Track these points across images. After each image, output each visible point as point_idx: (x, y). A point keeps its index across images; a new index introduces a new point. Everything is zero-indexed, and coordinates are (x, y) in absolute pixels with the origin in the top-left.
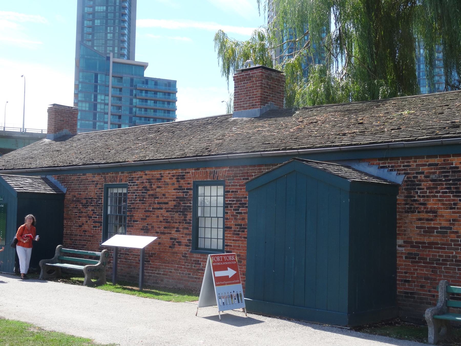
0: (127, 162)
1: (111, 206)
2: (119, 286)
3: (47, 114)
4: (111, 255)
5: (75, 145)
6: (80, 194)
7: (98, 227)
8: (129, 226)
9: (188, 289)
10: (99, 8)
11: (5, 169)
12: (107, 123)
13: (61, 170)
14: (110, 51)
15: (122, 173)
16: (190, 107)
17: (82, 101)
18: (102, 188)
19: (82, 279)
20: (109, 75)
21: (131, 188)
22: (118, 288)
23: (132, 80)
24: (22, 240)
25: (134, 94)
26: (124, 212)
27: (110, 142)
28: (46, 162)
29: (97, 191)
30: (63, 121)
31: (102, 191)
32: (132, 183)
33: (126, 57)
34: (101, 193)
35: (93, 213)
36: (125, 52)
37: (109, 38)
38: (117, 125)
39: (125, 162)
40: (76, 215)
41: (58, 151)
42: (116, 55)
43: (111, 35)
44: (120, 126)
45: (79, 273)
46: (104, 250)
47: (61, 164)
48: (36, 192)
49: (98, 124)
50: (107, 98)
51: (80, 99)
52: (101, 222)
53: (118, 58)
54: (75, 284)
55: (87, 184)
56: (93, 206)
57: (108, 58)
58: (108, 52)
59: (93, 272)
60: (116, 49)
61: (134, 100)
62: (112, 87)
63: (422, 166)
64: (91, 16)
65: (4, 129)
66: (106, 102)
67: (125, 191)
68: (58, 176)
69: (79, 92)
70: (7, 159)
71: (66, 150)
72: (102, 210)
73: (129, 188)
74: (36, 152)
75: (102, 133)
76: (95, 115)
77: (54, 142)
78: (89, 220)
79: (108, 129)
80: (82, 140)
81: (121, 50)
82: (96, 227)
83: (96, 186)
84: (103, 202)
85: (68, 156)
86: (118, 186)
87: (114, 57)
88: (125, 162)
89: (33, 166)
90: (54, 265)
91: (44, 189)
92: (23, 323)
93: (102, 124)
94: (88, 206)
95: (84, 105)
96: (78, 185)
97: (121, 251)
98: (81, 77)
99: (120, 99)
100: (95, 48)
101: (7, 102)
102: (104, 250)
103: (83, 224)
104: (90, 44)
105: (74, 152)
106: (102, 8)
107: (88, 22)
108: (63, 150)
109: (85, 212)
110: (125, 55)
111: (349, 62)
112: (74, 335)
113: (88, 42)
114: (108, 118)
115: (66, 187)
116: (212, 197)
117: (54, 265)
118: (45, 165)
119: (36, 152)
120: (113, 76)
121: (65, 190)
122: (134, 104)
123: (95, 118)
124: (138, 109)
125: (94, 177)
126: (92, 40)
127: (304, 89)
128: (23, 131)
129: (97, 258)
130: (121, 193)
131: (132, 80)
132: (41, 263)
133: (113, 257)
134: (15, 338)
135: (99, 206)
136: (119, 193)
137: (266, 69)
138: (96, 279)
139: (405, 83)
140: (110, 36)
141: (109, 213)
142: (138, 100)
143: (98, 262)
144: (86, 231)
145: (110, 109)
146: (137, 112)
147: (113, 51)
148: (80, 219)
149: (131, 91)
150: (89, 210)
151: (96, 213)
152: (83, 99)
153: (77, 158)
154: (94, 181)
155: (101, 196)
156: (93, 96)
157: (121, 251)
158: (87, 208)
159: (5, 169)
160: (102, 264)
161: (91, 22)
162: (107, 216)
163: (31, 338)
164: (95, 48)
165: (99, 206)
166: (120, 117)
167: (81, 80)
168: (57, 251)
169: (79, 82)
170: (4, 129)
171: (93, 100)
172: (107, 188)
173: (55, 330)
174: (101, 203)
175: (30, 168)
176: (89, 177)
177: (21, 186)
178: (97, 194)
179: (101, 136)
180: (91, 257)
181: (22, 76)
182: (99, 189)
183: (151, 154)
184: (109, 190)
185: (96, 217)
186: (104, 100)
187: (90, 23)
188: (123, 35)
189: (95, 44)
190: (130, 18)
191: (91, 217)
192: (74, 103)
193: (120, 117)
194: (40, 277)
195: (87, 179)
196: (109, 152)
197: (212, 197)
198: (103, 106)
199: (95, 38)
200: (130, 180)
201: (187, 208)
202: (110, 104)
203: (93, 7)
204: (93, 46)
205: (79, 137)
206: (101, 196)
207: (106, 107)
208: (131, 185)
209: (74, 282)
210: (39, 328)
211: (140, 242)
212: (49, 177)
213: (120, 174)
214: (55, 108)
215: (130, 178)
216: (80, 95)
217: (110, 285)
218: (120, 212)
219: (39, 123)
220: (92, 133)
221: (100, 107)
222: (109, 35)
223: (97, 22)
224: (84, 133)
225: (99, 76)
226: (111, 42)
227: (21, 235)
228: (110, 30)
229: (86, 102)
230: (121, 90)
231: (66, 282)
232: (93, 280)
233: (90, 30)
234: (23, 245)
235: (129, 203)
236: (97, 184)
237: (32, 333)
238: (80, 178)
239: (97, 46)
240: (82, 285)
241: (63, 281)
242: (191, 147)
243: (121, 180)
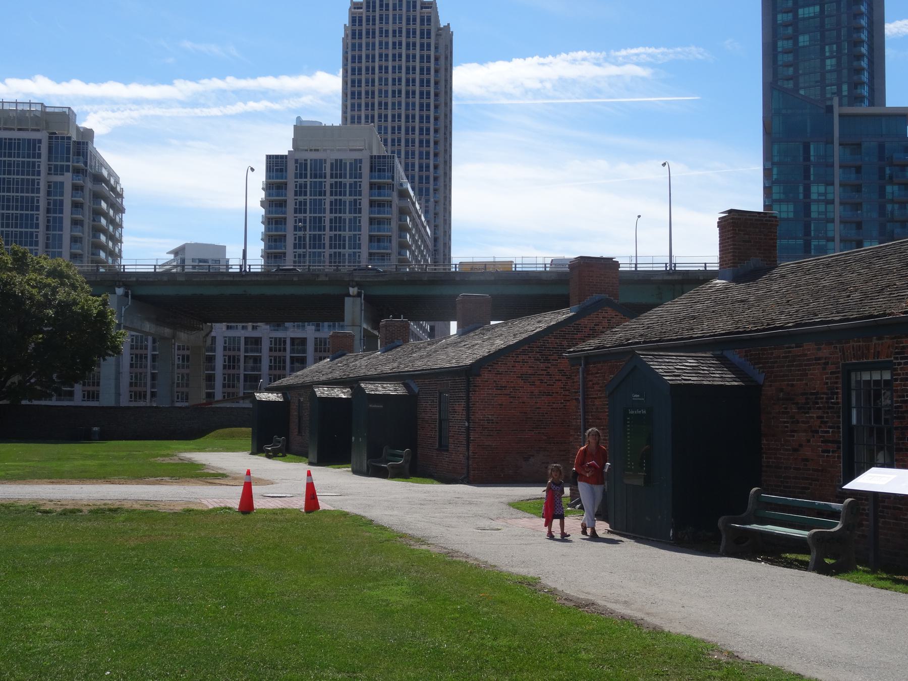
0: (890, 315)
1: (859, 408)
2: (885, 576)
3: (717, 231)
4: (864, 509)
5: (775, 287)
6: (792, 385)
7: (833, 452)
8: (899, 450)
10: (806, 9)
11: (645, 342)
12: (832, 239)
13: (752, 339)
14: (834, 93)
15: (879, 339)
17: (779, 201)
18: (838, 372)
19: (806, 558)
20: (832, 143)
21: (901, 369)
22: (883, 579)
23: (881, 147)
24: (583, 473)
25: (887, 176)
26: (886, 421)
27: (849, 276)
28: (722, 325)
29: (827, 378)
31: (837, 378)
32: (902, 358)
33: (866, 102)
34: (836, 383)
35: (822, 422)
36: (865, 91)
37: (828, 68)
38: (854, 243)
39: (885, 315)
40: (787, 427)
41: (742, 301)
42: (845, 100)
43: (834, 61)
44: (860, 244)
45: (798, 545)
46: (850, 500)
47: (750, 327)
48: (705, 383)
49: (814, 243)
50: (830, 188)
51: (775, 196)
52: (839, 442)
53: (850, 104)
54: (791, 568)
55: (806, 365)
56: (819, 408)
57: (830, 109)
58: (828, 96)
59: (824, 543)
60: (845, 87)
61: (889, 189)
62: (841, 167)
64: (790, 30)
65: (636, 267)
66: (830, 197)
67: (887, 376)
68: (746, 352)
69: (773, 183)
70: (646, 322)
71: (759, 299)
72: (839, 417)
73: (896, 370)
74: (699, 306)
75: (830, 260)
76: (807, 227)
77: (732, 285)
78: (813, 436)
79: (835, 253)
80: (790, 276)
81: (856, 88)
82: (828, 452)
83: (824, 369)
84: (840, 401)
85: (764, 311)
86: (871, 367)
87: (841, 105)
88: (885, 315)
89: (698, 333)
90: (748, 527)
91: (720, 377)
92: (697, 641)
93: (823, 242)
94: (809, 408)
95: (784, 207)
96: (788, 366)
97: (884, 502)
98: (775, 152)
99: (858, 188)
100: (802, 92)
101: (639, 216)
102: (850, 500)
103: (801, 446)
104: (790, 85)
105: (772, 303)
106: (811, 9)
107: (785, 42)
108: (752, 298)
109: (803, 422)
110: (864, 97)
111: (204, 404)
112: (802, 674)
113: (786, 82)
114: (836, 230)
115: (763, 372)
117: (748, 527)
118: (719, 331)
119: (699, 306)
120: (840, 145)
121: (761, 378)
122: (889, 196)
123: (807, 232)
124: (896, 206)
125: (819, 349)
126: (794, 78)
128: (671, 269)
129: (835, 514)
130: (869, 381)
131: (881, 147)
132: (720, 522)
133: (867, 515)
134: (686, 670)
135: (833, 408)
136: (885, 381)
138: (834, 556)
140: (830, 63)
141: (854, 422)
142: (896, 188)
143: (836, 524)
144: (807, 460)
145: (837, 211)
146: (896, 213)
147: (839, 93)
148: (793, 436)
149: (882, 170)
150: (812, 417)
151: (826, 422)
152: (782, 196)
153: (782, 313)
154: (819, 359)
155: (837, 388)
156: (801, 189)
157: (884, 502)
158: (808, 413)
159: (645, 342)
160: (845, 527)
161: (791, 42)
162: (850, 429)
163: (715, 673)
164: (802, 92)
165: (833, 408)
166: (859, 225)
167: (776, 159)
168: (751, 500)
169: (773, 164)
170: (636, 267)
171: (801, 196)
172: (848, 370)
173: (763, 660)
174: (838, 403)
175: (691, 338)
176: (809, 350)
177: (677, 372)
178: (827, 383)
179: (828, 265)
180: (821, 512)
181: (664, 164)
182: (832, 373)
184: (853, 375)
185: (827, 432)
186: (825, 194)
187: (789, 44)
188: (860, 57)
189: (801, 85)
190: (871, 23)
191: (817, 432)
192: (765, 206)
193: (859, 225)
194: (721, 550)
195: (806, 355)
196: (849, 296)
198: (822, 208)
199: (801, 72)
200: (897, 353)
202: (837, 201)
203: (794, 11)
204: (797, 88)
205: (783, 271)
206: (837, 388)
207: (830, 207)
208: (900, 364)
209: (788, 563)
210: (729, 653)
212: (726, 353)
213: (875, 341)
214: (732, 219)
215: (896, 348)
216: (775, 189)
217: (864, 571)
218: (878, 419)
219: (701, 249)
220: (809, 262)
221: (815, 210)
222: (828, 62)
223: (804, 40)
224: (791, 264)
225: (812, 147)
226: (834, 75)
227: (581, 464)
228: (831, 51)
229: (786, 201)
230: (858, 170)
231: (773, 563)
232: (827, 561)
233: (790, 58)
234: (587, 480)
235: (897, 402)
236: (826, 364)
237: (718, 662)
238: (790, 352)
239: (804, 88)
240: (806, 570)
241: (766, 561)
243: (878, 354)
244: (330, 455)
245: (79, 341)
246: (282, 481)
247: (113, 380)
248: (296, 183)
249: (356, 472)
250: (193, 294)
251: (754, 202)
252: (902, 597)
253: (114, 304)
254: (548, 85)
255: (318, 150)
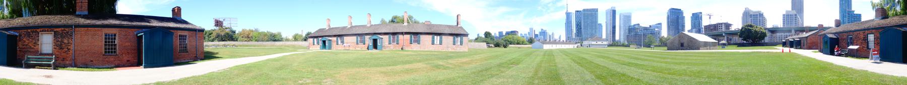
9: (867, 57)
16: (864, 18)
30: (838, 24)
63: (23, 31)
105: (840, 29)
116: (871, 37)
127: (891, 13)
137: (882, 8)
138: (847, 55)
139: (20, 15)
183: (857, 28)
197: (871, 37)
201: (866, 39)
211: (856, 47)
219: (833, 25)
242: (866, 26)
244: (792, 46)
245: (763, 35)
246: (787, 50)
247: (767, 40)
248: (787, 17)
249: (145, 67)
250: (773, 31)
251: (863, 19)
252: (2, 77)
253: (767, 31)
254: (47, 42)
255: (274, 38)
